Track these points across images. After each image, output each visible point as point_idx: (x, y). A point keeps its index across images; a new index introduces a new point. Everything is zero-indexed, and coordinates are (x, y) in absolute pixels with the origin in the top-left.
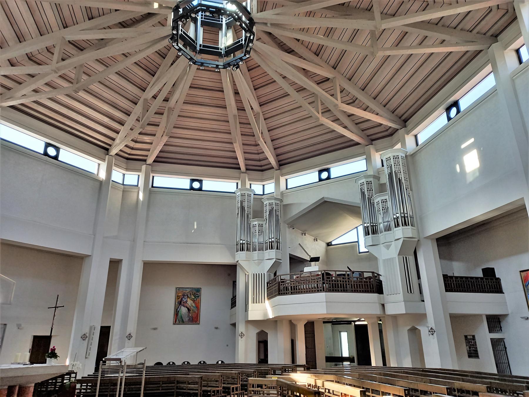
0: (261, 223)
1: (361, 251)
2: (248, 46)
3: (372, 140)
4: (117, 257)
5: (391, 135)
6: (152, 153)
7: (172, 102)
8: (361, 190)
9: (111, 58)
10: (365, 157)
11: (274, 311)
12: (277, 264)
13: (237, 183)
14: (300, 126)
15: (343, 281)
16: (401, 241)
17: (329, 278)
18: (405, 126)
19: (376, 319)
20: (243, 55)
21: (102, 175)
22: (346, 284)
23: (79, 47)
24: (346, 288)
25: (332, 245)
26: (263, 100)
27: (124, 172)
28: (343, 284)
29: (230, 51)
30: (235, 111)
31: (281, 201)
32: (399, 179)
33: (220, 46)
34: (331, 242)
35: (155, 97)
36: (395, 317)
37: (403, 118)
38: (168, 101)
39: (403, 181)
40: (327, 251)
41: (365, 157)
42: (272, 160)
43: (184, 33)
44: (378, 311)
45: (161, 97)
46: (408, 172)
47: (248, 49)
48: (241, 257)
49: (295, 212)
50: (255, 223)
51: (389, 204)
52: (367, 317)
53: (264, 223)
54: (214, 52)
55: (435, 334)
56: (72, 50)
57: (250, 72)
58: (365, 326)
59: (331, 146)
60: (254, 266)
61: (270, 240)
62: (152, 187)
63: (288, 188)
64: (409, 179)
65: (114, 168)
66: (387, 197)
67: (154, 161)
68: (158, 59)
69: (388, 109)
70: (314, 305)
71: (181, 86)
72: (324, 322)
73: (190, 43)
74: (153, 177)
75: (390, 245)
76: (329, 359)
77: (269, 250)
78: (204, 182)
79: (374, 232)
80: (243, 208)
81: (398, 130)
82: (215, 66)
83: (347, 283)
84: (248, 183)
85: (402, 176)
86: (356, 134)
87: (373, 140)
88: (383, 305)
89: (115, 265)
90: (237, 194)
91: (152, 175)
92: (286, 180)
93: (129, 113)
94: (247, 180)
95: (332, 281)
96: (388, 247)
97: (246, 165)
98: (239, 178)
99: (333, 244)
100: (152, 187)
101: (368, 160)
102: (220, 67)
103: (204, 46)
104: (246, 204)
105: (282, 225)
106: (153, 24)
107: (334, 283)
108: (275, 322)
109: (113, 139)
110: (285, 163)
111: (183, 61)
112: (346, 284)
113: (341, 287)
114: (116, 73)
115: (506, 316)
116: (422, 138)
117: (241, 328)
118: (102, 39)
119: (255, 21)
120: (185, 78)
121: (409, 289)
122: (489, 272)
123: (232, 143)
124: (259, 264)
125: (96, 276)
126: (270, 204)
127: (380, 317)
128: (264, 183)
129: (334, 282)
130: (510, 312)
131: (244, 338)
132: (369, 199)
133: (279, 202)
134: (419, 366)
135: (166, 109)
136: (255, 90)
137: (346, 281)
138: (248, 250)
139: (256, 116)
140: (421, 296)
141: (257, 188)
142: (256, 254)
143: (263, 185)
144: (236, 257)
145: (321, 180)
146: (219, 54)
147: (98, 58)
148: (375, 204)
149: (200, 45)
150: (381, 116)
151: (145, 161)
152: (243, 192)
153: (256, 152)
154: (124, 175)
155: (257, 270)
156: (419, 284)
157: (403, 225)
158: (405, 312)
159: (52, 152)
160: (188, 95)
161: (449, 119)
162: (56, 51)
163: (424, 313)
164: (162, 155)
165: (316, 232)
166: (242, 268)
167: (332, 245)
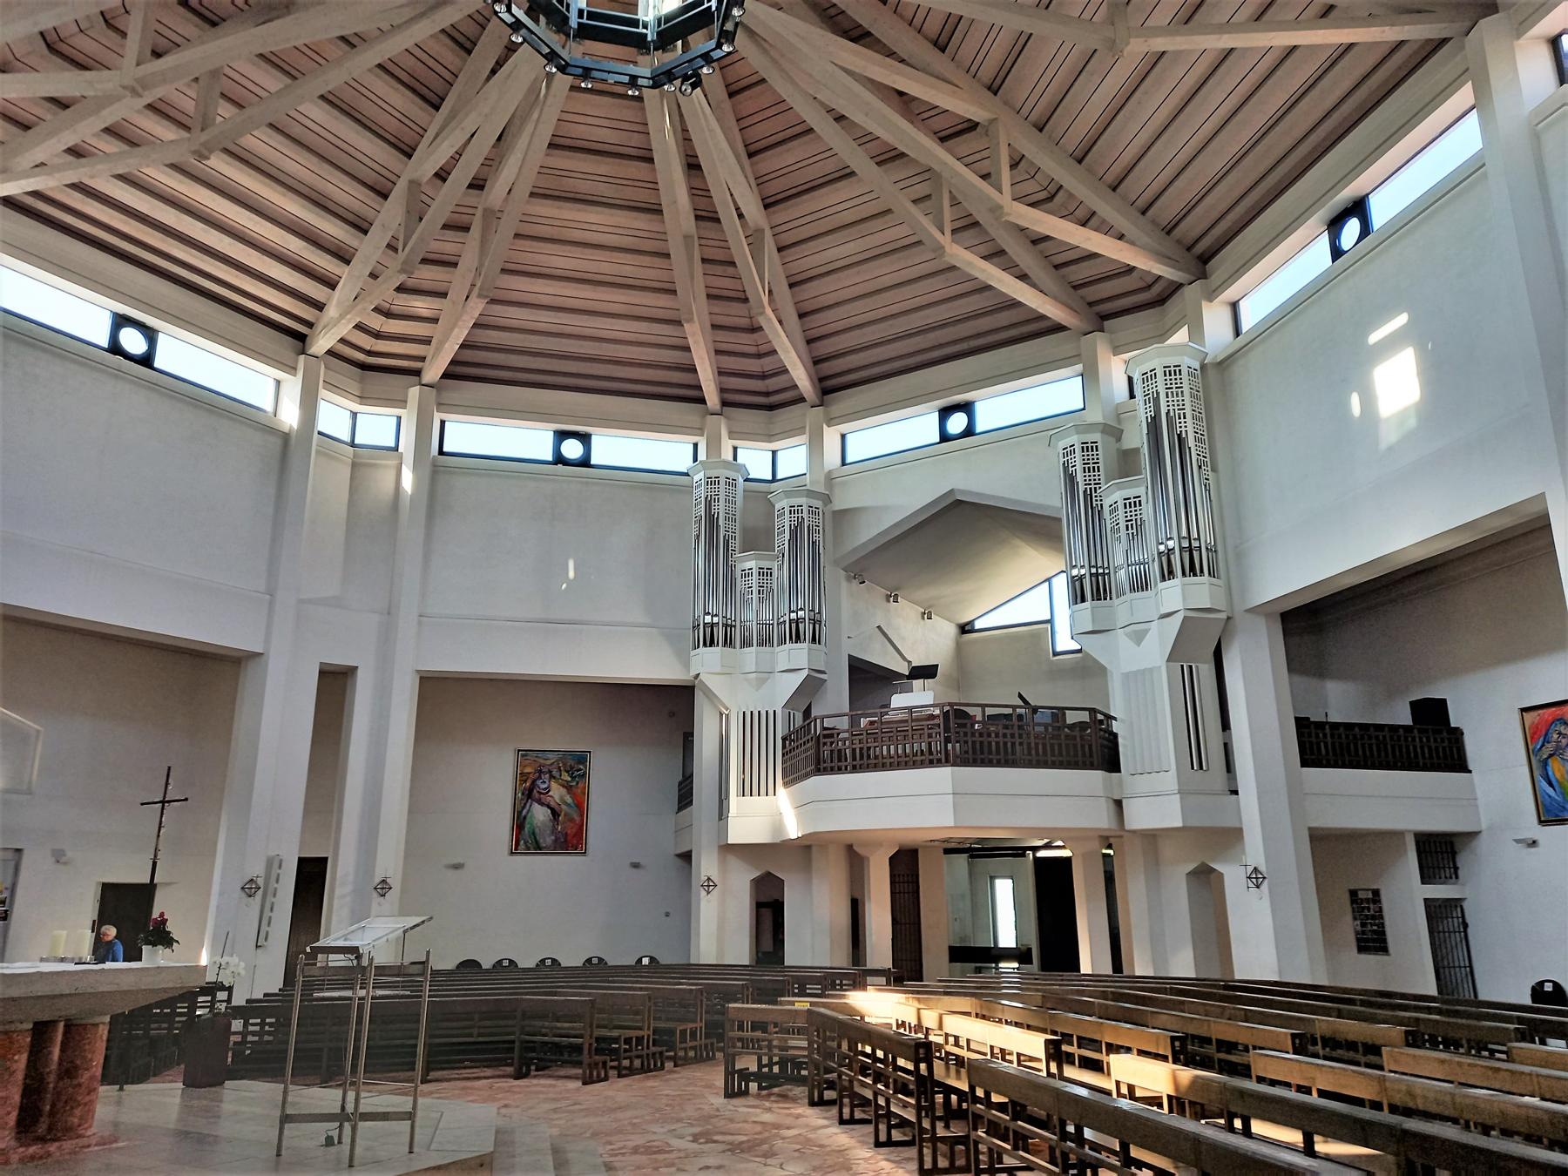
1: (1059, 649)
3: (1102, 316)
4: (339, 659)
8: (1066, 469)
9: (305, 50)
10: (1079, 367)
11: (801, 818)
12: (812, 685)
13: (696, 446)
14: (885, 271)
16: (1176, 622)
17: (964, 725)
19: (1096, 844)
20: (713, 44)
21: (290, 417)
24: (1014, 753)
27: (356, 407)
30: (688, 223)
31: (827, 499)
32: (1179, 436)
33: (641, 16)
34: (971, 622)
35: (442, 175)
36: (1152, 838)
37: (1200, 248)
38: (481, 188)
39: (1191, 442)
40: (959, 647)
41: (1079, 367)
42: (801, 377)
44: (1101, 819)
46: (1207, 415)
47: (729, 26)
48: (707, 665)
49: (867, 532)
50: (752, 564)
52: (1071, 835)
55: (1265, 886)
60: (746, 690)
62: (441, 452)
64: (1208, 438)
65: (323, 393)
66: (1141, 491)
69: (1153, 222)
70: (917, 802)
71: (522, 143)
74: (443, 423)
75: (1147, 631)
77: (788, 645)
78: (980, 409)
79: (1101, 592)
80: (711, 520)
81: (1181, 285)
82: (626, 79)
83: (1018, 741)
84: (727, 445)
85: (1188, 428)
86: (1055, 298)
88: (1119, 804)
89: (335, 684)
90: (696, 478)
92: (843, 436)
95: (973, 734)
96: (1139, 638)
97: (722, 390)
98: (700, 431)
100: (441, 452)
101: (1090, 378)
103: (591, 16)
104: (720, 509)
105: (832, 575)
107: (970, 738)
108: (805, 850)
109: (319, 306)
110: (840, 383)
111: (527, 64)
112: (1013, 744)
114: (322, 97)
115: (1473, 835)
117: (707, 865)
120: (535, 116)
121: (1196, 756)
122: (1432, 713)
124: (761, 682)
125: (280, 715)
130: (1484, 826)
131: (715, 893)
132: (1088, 496)
134: (1215, 973)
135: (479, 213)
137: (1013, 736)
138: (728, 642)
139: (754, 239)
143: (774, 453)
145: (945, 437)
146: (639, 42)
148: (1106, 510)
149: (581, 12)
151: (417, 373)
152: (713, 473)
153: (753, 350)
154: (354, 415)
157: (1184, 574)
158: (1180, 824)
159: (133, 341)
160: (544, 170)
161: (1337, 253)
164: (470, 355)
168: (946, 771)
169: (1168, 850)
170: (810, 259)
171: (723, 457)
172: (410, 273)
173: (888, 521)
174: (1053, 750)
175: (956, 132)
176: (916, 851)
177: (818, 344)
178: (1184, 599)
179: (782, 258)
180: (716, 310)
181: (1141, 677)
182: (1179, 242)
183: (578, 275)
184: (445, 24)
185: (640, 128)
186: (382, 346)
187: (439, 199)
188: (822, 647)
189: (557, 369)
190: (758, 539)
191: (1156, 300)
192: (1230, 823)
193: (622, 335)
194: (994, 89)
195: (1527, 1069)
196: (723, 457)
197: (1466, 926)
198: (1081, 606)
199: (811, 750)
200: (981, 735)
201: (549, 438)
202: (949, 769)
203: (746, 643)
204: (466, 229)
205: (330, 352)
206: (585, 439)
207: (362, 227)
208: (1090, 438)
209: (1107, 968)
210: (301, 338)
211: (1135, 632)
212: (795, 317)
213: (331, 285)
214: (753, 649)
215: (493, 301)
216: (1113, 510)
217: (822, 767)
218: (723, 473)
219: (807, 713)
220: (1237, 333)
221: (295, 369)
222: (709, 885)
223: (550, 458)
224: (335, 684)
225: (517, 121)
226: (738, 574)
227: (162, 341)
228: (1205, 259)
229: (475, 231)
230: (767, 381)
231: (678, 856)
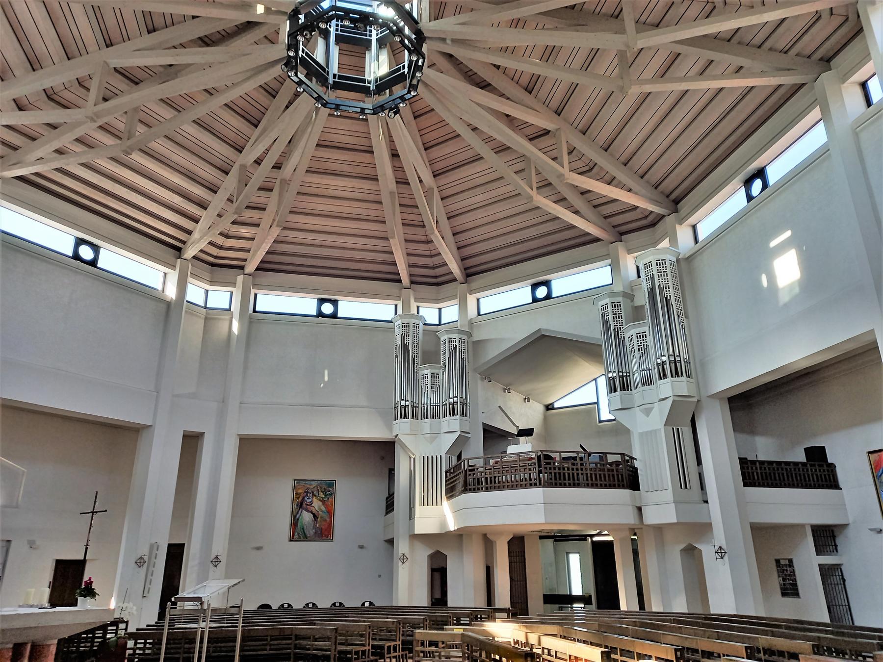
0: (435, 371)
1: (602, 419)
2: (413, 76)
3: (621, 233)
4: (195, 428)
5: (653, 225)
6: (254, 255)
7: (287, 170)
8: (603, 317)
9: (185, 96)
10: (609, 261)
11: (457, 519)
12: (462, 440)
13: (396, 306)
14: (501, 210)
15: (573, 469)
16: (669, 402)
17: (549, 464)
19: (628, 533)
20: (406, 91)
21: (171, 293)
22: (578, 474)
23: (132, 78)
24: (578, 480)
25: (553, 409)
26: (439, 166)
27: (208, 287)
28: (573, 474)
29: (384, 84)
30: (393, 186)
31: (470, 335)
32: (666, 298)
33: (366, 77)
34: (552, 404)
35: (258, 162)
36: (659, 529)
37: (673, 196)
38: (280, 168)
39: (673, 302)
40: (545, 419)
41: (609, 261)
42: (455, 268)
43: (307, 54)
44: (630, 519)
45: (268, 162)
46: (681, 287)
47: (414, 82)
48: (402, 429)
49: (492, 353)
50: (425, 372)
51: (650, 340)
52: (613, 528)
53: (441, 372)
54: (358, 86)
56: (120, 83)
57: (418, 119)
58: (610, 544)
59: (553, 244)
60: (424, 444)
61: (451, 401)
62: (254, 311)
63: (481, 313)
64: (682, 298)
65: (190, 279)
66: (646, 329)
67: (258, 269)
68: (263, 99)
69: (648, 182)
70: (524, 508)
71: (302, 144)
72: (541, 537)
73: (317, 72)
74: (256, 295)
75: (651, 409)
76: (549, 599)
77: (448, 417)
78: (341, 304)
79: (625, 387)
80: (405, 347)
81: (664, 216)
82: (359, 110)
83: (580, 472)
84: (414, 305)
85: (671, 294)
86: (594, 224)
87: (622, 234)
88: (640, 509)
90: (396, 324)
91: (253, 292)
92: (478, 300)
93: (216, 189)
94: (412, 301)
95: (555, 469)
96: (648, 412)
97: (411, 275)
98: (398, 297)
99: (556, 406)
100: (254, 311)
101: (615, 267)
102: (366, 111)
103: (340, 77)
104: (410, 341)
105: (471, 375)
106: (256, 39)
107: (557, 471)
108: (459, 537)
109: (189, 233)
110: (476, 271)
111: (305, 102)
112: (578, 474)
113: (569, 479)
114: (194, 121)
116: (705, 230)
117: (402, 547)
118: (171, 65)
119: (426, 35)
120: (309, 130)
121: (683, 482)
123: (387, 239)
124: (432, 440)
126: (451, 341)
127: (634, 529)
128: (440, 305)
129: (557, 471)
131: (407, 563)
132: (616, 332)
133: (465, 337)
134: (699, 610)
135: (278, 182)
136: (426, 149)
137: (577, 469)
138: (414, 416)
139: (428, 193)
140: (702, 494)
141: (429, 313)
142: (427, 424)
143: (440, 309)
144: (394, 429)
145: (535, 300)
146: (366, 91)
147: (163, 97)
148: (627, 340)
149: (335, 76)
150: (636, 194)
151: (242, 268)
152: (405, 321)
153: (427, 253)
154: (207, 291)
155: (430, 451)
156: (700, 474)
157: (672, 376)
158: (675, 521)
159: (86, 253)
160: (314, 158)
161: (750, 198)
162: (94, 86)
163: (708, 521)
164: (271, 258)
165: (527, 387)
166: (404, 447)
167: (553, 409)
175: (538, 136)
197: (844, 580)
206: (96, 249)
223: (70, 254)
224: (192, 442)
231: (386, 541)
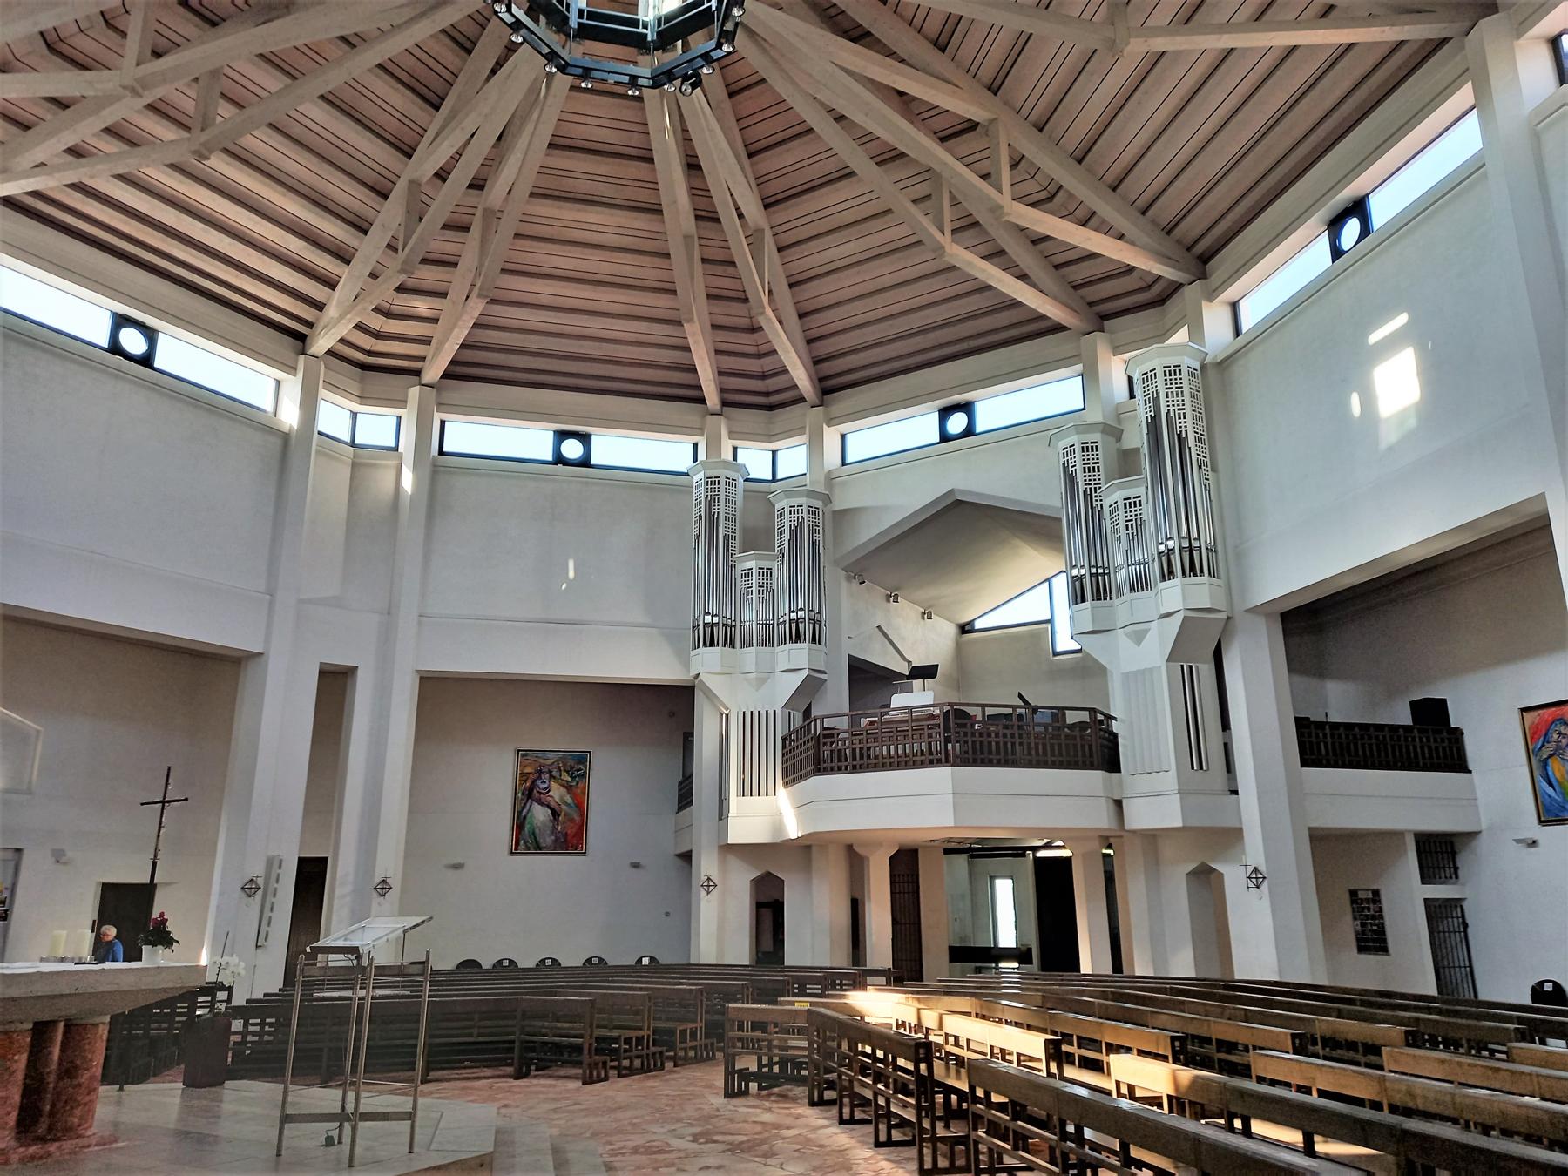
1: (1059, 649)
3: (1102, 316)
4: (339, 659)
8: (1066, 469)
9: (305, 50)
10: (1079, 367)
11: (801, 818)
12: (812, 685)
13: (696, 446)
14: (885, 271)
16: (1176, 622)
17: (964, 725)
18: (1204, 275)
19: (1096, 844)
20: (713, 44)
24: (1014, 753)
27: (356, 407)
30: (688, 223)
31: (827, 499)
32: (1179, 436)
33: (641, 16)
34: (971, 622)
35: (442, 175)
36: (1152, 838)
37: (1200, 248)
38: (481, 188)
39: (1191, 442)
40: (959, 647)
41: (1079, 367)
42: (801, 377)
44: (1101, 819)
46: (1207, 415)
47: (729, 26)
48: (707, 665)
49: (867, 532)
50: (752, 564)
52: (1071, 835)
55: (1265, 886)
60: (746, 690)
62: (441, 452)
64: (1208, 438)
65: (323, 393)
66: (1141, 491)
69: (1153, 222)
70: (917, 802)
74: (443, 423)
75: (1147, 631)
77: (788, 645)
78: (980, 409)
79: (1101, 592)
80: (711, 520)
82: (626, 79)
83: (1018, 741)
84: (727, 445)
85: (1188, 428)
86: (1055, 298)
88: (1119, 804)
89: (335, 684)
90: (696, 478)
92: (843, 436)
95: (973, 734)
96: (1139, 638)
97: (722, 390)
98: (700, 431)
100: (441, 452)
101: (1090, 378)
103: (591, 16)
104: (720, 509)
105: (832, 575)
107: (970, 738)
108: (805, 850)
109: (319, 306)
110: (840, 383)
111: (527, 64)
112: (1013, 744)
114: (322, 97)
115: (1473, 835)
117: (707, 865)
121: (1196, 756)
122: (1432, 713)
124: (761, 682)
130: (1484, 826)
131: (715, 893)
132: (1088, 496)
134: (1215, 973)
135: (479, 213)
137: (1013, 736)
138: (728, 642)
139: (754, 239)
143: (774, 453)
145: (945, 437)
146: (639, 42)
148: (1106, 510)
149: (581, 12)
151: (417, 373)
152: (713, 473)
153: (753, 350)
154: (354, 415)
157: (1184, 574)
158: (1180, 824)
159: (133, 341)
160: (544, 170)
161: (1337, 253)
164: (470, 355)
168: (946, 771)
169: (1168, 850)
170: (810, 259)
171: (723, 457)
172: (410, 273)
173: (888, 521)
174: (1053, 750)
175: (956, 132)
176: (916, 851)
177: (818, 344)
178: (1184, 599)
179: (782, 258)
180: (716, 310)
181: (1141, 677)
182: (1179, 242)
183: (578, 275)
184: (445, 24)
185: (640, 128)
186: (382, 346)
187: (439, 199)
188: (822, 647)
189: (557, 369)
190: (758, 539)
191: (1156, 300)
192: (1230, 823)
193: (622, 335)
194: (994, 89)
195: (1527, 1069)
196: (723, 457)
198: (1081, 606)
199: (811, 750)
200: (981, 735)
201: (549, 438)
202: (949, 769)
203: (746, 643)
204: (466, 229)
205: (330, 352)
206: (585, 439)
207: (362, 227)
208: (1090, 438)
209: (1107, 968)
210: (301, 338)
211: (1135, 632)
212: (795, 317)
213: (331, 285)
214: (753, 649)
215: (493, 301)
216: (1113, 510)
217: (822, 767)
218: (723, 473)
219: (807, 713)
220: (1237, 333)
221: (295, 369)
222: (709, 885)
223: (550, 458)
224: (335, 684)
225: (517, 121)
226: (738, 574)
227: (162, 341)
228: (1205, 259)
229: (475, 231)
230: (767, 381)
